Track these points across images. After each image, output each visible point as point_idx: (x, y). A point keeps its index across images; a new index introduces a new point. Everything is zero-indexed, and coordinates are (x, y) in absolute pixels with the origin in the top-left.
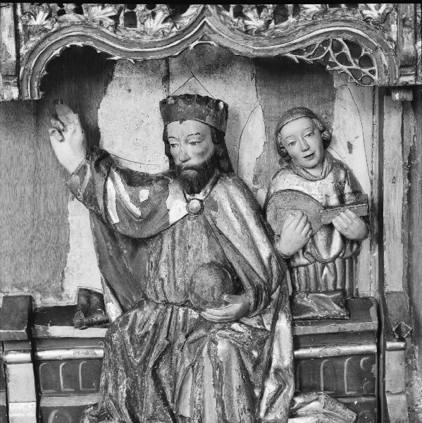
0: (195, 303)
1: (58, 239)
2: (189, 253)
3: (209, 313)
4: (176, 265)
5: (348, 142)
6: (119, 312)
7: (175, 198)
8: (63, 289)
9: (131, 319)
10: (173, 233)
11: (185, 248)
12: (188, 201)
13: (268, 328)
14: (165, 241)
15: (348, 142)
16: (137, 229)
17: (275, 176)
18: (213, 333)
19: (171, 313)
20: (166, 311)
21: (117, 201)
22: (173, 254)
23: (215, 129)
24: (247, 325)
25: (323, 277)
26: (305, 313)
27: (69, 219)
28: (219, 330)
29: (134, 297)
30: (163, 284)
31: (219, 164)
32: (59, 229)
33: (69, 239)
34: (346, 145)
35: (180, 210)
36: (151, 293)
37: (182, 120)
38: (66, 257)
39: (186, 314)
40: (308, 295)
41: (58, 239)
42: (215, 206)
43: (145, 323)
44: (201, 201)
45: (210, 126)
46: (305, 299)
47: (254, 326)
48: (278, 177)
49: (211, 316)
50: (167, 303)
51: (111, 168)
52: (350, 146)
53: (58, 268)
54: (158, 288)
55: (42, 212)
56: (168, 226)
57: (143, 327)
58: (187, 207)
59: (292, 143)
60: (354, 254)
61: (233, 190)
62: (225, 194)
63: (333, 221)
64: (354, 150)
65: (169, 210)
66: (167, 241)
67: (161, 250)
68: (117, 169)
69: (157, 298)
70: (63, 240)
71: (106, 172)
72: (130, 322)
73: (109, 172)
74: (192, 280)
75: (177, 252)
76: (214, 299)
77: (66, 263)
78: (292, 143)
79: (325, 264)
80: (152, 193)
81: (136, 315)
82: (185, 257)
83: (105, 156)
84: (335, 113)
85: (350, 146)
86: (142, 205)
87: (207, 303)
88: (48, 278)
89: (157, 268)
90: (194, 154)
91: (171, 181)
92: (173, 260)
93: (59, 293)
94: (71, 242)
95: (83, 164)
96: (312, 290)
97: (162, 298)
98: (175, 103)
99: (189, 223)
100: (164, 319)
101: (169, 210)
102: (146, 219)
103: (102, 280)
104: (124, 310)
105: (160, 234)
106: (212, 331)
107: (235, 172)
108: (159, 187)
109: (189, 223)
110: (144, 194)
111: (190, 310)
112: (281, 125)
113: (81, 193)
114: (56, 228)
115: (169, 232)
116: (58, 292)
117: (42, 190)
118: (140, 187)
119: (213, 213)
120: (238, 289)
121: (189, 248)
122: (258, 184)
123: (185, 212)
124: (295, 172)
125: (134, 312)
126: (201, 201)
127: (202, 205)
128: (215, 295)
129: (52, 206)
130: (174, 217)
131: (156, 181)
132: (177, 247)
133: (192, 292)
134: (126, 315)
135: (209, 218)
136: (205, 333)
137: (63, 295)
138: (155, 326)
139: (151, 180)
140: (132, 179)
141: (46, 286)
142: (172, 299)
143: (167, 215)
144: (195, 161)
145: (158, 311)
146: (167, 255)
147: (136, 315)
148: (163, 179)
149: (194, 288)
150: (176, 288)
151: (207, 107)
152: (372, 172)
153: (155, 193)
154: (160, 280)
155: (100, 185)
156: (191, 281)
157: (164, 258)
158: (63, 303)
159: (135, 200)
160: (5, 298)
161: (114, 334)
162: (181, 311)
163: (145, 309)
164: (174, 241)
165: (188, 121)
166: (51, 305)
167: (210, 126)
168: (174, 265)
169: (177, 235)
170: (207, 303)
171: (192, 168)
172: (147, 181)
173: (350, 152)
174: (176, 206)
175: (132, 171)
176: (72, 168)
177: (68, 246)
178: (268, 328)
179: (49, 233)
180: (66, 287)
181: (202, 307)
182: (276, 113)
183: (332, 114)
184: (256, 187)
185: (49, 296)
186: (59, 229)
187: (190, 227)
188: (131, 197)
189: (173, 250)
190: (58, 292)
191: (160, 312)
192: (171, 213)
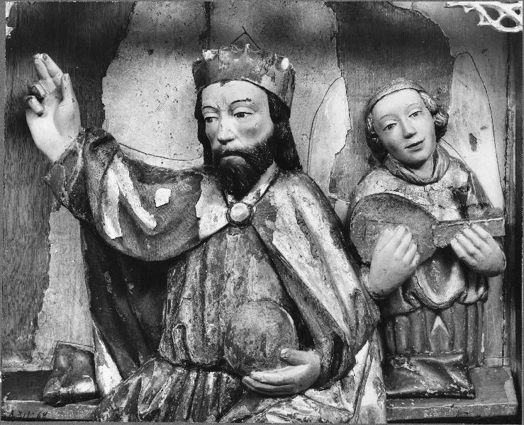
0: (233, 361)
1: (32, 268)
2: (228, 285)
3: (256, 380)
4: (207, 303)
5: (471, 134)
6: (118, 379)
7: (210, 201)
8: (34, 346)
9: (131, 388)
10: (205, 254)
11: (222, 277)
12: (229, 206)
13: (350, 407)
14: (191, 266)
15: (471, 134)
16: (149, 246)
17: (363, 178)
18: (262, 411)
19: (196, 381)
20: (187, 377)
21: (120, 203)
22: (202, 286)
23: (276, 97)
24: (315, 401)
25: (433, 333)
26: (406, 386)
27: (50, 237)
28: (270, 406)
29: (141, 357)
30: (184, 333)
31: (280, 154)
32: (33, 254)
33: (48, 269)
34: (467, 139)
35: (216, 219)
36: (166, 349)
37: (224, 81)
38: (43, 295)
39: (218, 382)
40: (409, 359)
41: (32, 268)
42: (272, 213)
43: (153, 396)
44: (250, 207)
45: (268, 92)
46: (406, 365)
47: (327, 402)
48: (366, 180)
49: (42, 65)
50: (189, 365)
51: (116, 157)
52: (473, 140)
53: (29, 312)
54: (177, 341)
55: (10, 227)
56: (199, 243)
57: (150, 402)
58: (228, 215)
59: (390, 126)
60: (480, 299)
61: (301, 192)
62: (287, 196)
63: (454, 243)
64: (479, 145)
65: (199, 219)
66: (194, 266)
67: (184, 282)
68: (125, 160)
69: (174, 356)
70: (40, 269)
71: (106, 161)
72: (130, 394)
73: (111, 161)
74: (230, 324)
75: (208, 284)
76: (265, 354)
77: (41, 306)
78: (390, 126)
79: (438, 311)
80: (174, 194)
81: (139, 384)
82: (219, 290)
83: (107, 139)
84: (453, 92)
85: (473, 140)
86: (158, 211)
87: (253, 361)
88: (12, 327)
89: (177, 308)
90: (240, 131)
91: (205, 177)
92: (202, 296)
93: (27, 352)
94: (51, 273)
95: (71, 148)
96: (417, 350)
97: (181, 356)
98: (215, 57)
99: (229, 238)
100: (183, 390)
101: (199, 219)
102: (162, 233)
103: (94, 331)
104: (124, 375)
105: (181, 259)
106: (260, 408)
107: (305, 170)
108: (186, 185)
109: (229, 238)
110: (162, 195)
111: (225, 375)
112: (373, 102)
113: (66, 193)
114: (30, 252)
115: (198, 253)
116: (27, 349)
117: (13, 195)
118: (157, 185)
119: (268, 223)
120: (306, 340)
121: (229, 276)
122: (336, 192)
123: (223, 222)
124: (392, 173)
125: (138, 378)
126: (250, 207)
127: (251, 211)
128: (267, 349)
129: (26, 218)
130: (205, 229)
131: (182, 178)
132: (210, 276)
133: (229, 344)
134: (126, 383)
135: (261, 231)
136: (248, 412)
137: (34, 354)
138: (170, 400)
139: (174, 177)
140: (142, 174)
141: (10, 339)
142: (196, 359)
143: (196, 225)
144: (241, 143)
145: (175, 376)
146: (193, 288)
147: (139, 384)
148: (195, 177)
149: (232, 338)
150: (205, 339)
151: (264, 62)
152: (505, 179)
153: (179, 193)
154: (179, 327)
155: (95, 176)
156: (229, 328)
157: (187, 292)
158: (32, 368)
159: (147, 203)
160: (5, 376)
161: (105, 414)
162: (211, 377)
163: (155, 374)
164: (204, 266)
165: (232, 82)
166: (14, 370)
167: (268, 92)
168: (203, 303)
169: (210, 256)
170: (253, 361)
171: (237, 152)
172: (169, 177)
173: (474, 149)
174: (212, 214)
175: (147, 166)
176: (55, 154)
177: (46, 279)
178: (350, 407)
179: (18, 259)
180: (40, 341)
181: (245, 368)
182: (365, 89)
183: (448, 94)
184: (333, 195)
185: (11, 355)
186: (33, 254)
187: (231, 245)
188: (143, 200)
189: (203, 280)
190: (27, 349)
191: (178, 380)
192: (202, 224)
